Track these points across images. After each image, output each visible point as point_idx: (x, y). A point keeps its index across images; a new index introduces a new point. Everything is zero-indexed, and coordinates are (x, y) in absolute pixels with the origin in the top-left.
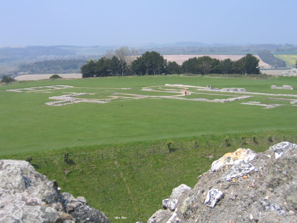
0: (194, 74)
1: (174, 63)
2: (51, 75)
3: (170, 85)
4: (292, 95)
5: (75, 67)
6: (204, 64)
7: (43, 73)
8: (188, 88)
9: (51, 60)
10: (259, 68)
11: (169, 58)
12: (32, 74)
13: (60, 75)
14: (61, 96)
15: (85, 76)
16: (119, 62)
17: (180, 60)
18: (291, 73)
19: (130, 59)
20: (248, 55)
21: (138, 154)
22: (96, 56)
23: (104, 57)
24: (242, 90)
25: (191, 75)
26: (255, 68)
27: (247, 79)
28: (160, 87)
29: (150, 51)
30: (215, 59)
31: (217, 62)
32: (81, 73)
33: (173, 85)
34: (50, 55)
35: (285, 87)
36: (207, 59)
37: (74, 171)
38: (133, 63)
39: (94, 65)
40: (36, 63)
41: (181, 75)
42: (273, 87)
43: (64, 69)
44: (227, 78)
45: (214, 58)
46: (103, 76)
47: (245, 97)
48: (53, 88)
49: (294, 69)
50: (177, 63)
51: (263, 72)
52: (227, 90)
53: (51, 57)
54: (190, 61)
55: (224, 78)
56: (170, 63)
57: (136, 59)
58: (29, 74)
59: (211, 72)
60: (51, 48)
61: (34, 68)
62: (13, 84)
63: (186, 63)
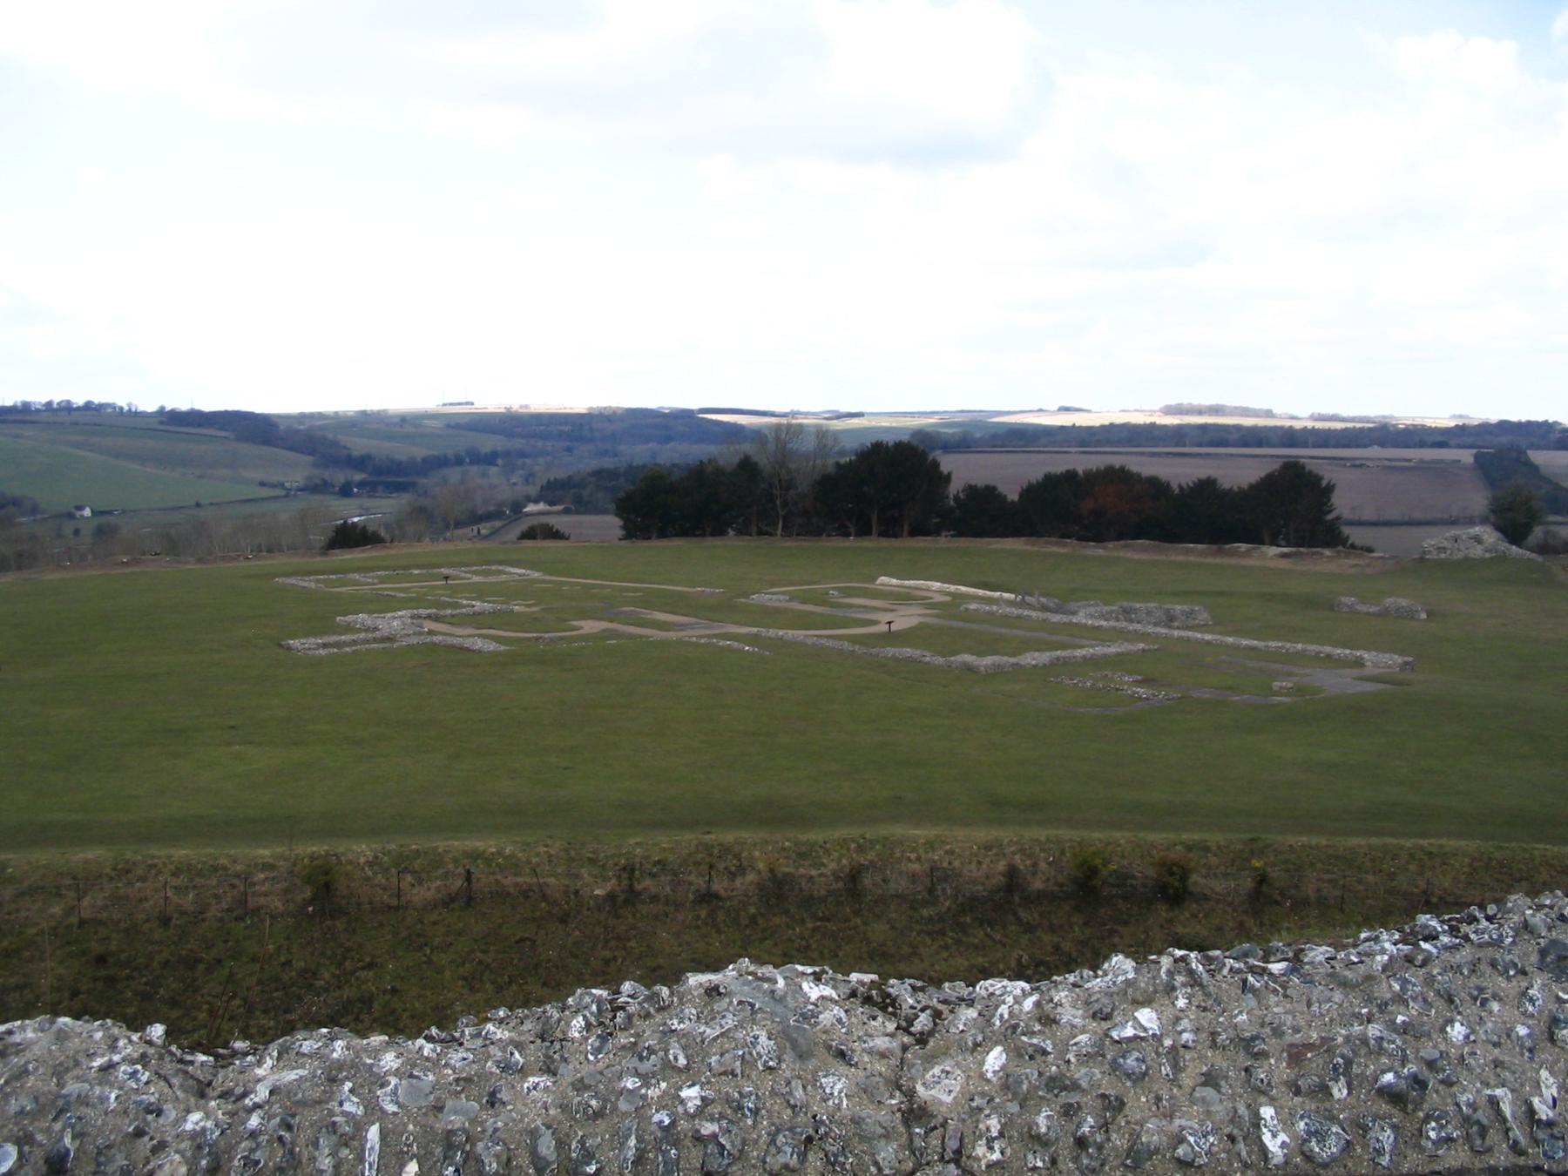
0: (1084, 543)
3: (894, 581)
8: (948, 599)
9: (674, 465)
10: (1338, 518)
11: (962, 472)
12: (578, 512)
14: (389, 615)
18: (1462, 547)
21: (192, 962)
23: (710, 461)
25: (337, 555)
28: (832, 589)
31: (1156, 487)
33: (907, 582)
34: (672, 445)
37: (720, 1074)
48: (446, 578)
49: (1477, 529)
50: (1002, 489)
54: (1051, 482)
56: (972, 491)
61: (586, 493)
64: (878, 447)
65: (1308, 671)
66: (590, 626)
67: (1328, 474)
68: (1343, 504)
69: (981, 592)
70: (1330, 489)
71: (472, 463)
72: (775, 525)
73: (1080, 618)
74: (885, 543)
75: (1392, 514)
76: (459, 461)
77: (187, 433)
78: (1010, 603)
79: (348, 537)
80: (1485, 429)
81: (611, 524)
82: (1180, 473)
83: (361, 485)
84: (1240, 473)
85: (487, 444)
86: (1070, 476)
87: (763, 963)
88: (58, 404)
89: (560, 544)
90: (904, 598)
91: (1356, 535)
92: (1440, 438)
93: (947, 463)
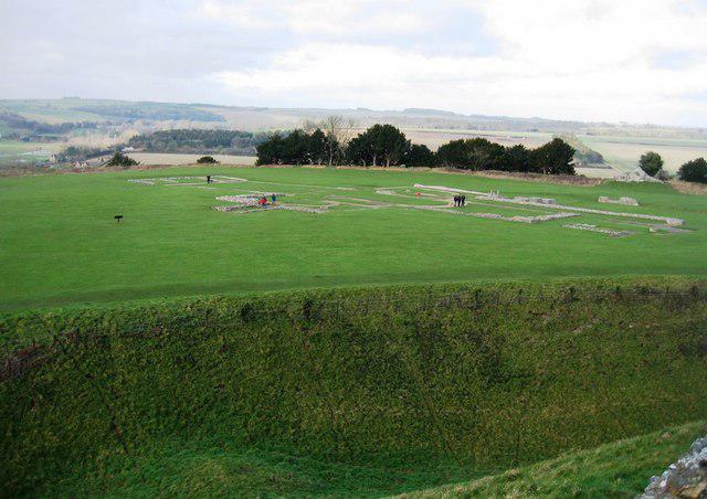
2: (199, 157)
4: (648, 217)
5: (245, 144)
6: (478, 152)
7: (168, 152)
11: (414, 137)
12: (150, 152)
13: (215, 157)
16: (326, 140)
19: (346, 135)
20: (556, 140)
22: (285, 125)
24: (550, 202)
26: (566, 164)
27: (545, 182)
29: (382, 124)
32: (258, 155)
35: (624, 200)
36: (481, 143)
38: (350, 143)
40: (156, 133)
41: (435, 170)
42: (603, 199)
43: (207, 146)
44: (517, 179)
45: (680, 166)
46: (294, 163)
47: (564, 215)
51: (578, 171)
52: (538, 201)
53: (182, 125)
55: (512, 178)
57: (356, 137)
58: (144, 151)
59: (488, 167)
60: (182, 106)
61: (153, 142)
62: (131, 171)
63: (444, 149)
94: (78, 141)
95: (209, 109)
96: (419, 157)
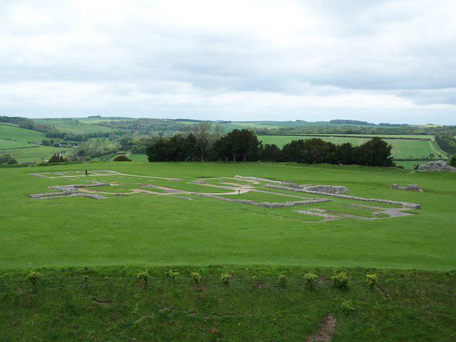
1: (274, 146)
11: (265, 140)
15: (151, 160)
17: (281, 142)
30: (329, 144)
39: (165, 145)
54: (294, 144)
64: (235, 131)
65: (384, 209)
66: (136, 191)
67: (389, 142)
68: (394, 154)
69: (270, 181)
70: (390, 147)
71: (100, 136)
72: (201, 158)
73: (304, 189)
74: (238, 164)
75: (404, 158)
76: (96, 136)
77: (401, 138)
78: (281, 185)
79: (56, 160)
80: (439, 129)
81: (145, 157)
82: (338, 141)
83: (62, 143)
84: (358, 142)
85: (105, 130)
86: (301, 142)
87: (314, 139)
88: (217, 128)
89: (129, 163)
90: (243, 183)
91: (398, 164)
92: (424, 132)
93: (260, 138)
94: (91, 145)
95: (184, 123)
96: (272, 155)
